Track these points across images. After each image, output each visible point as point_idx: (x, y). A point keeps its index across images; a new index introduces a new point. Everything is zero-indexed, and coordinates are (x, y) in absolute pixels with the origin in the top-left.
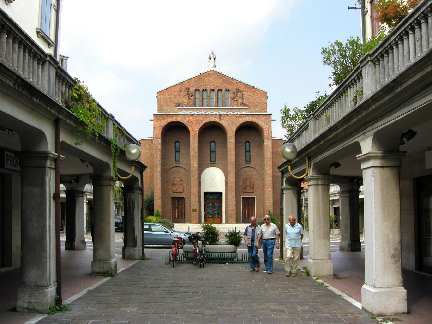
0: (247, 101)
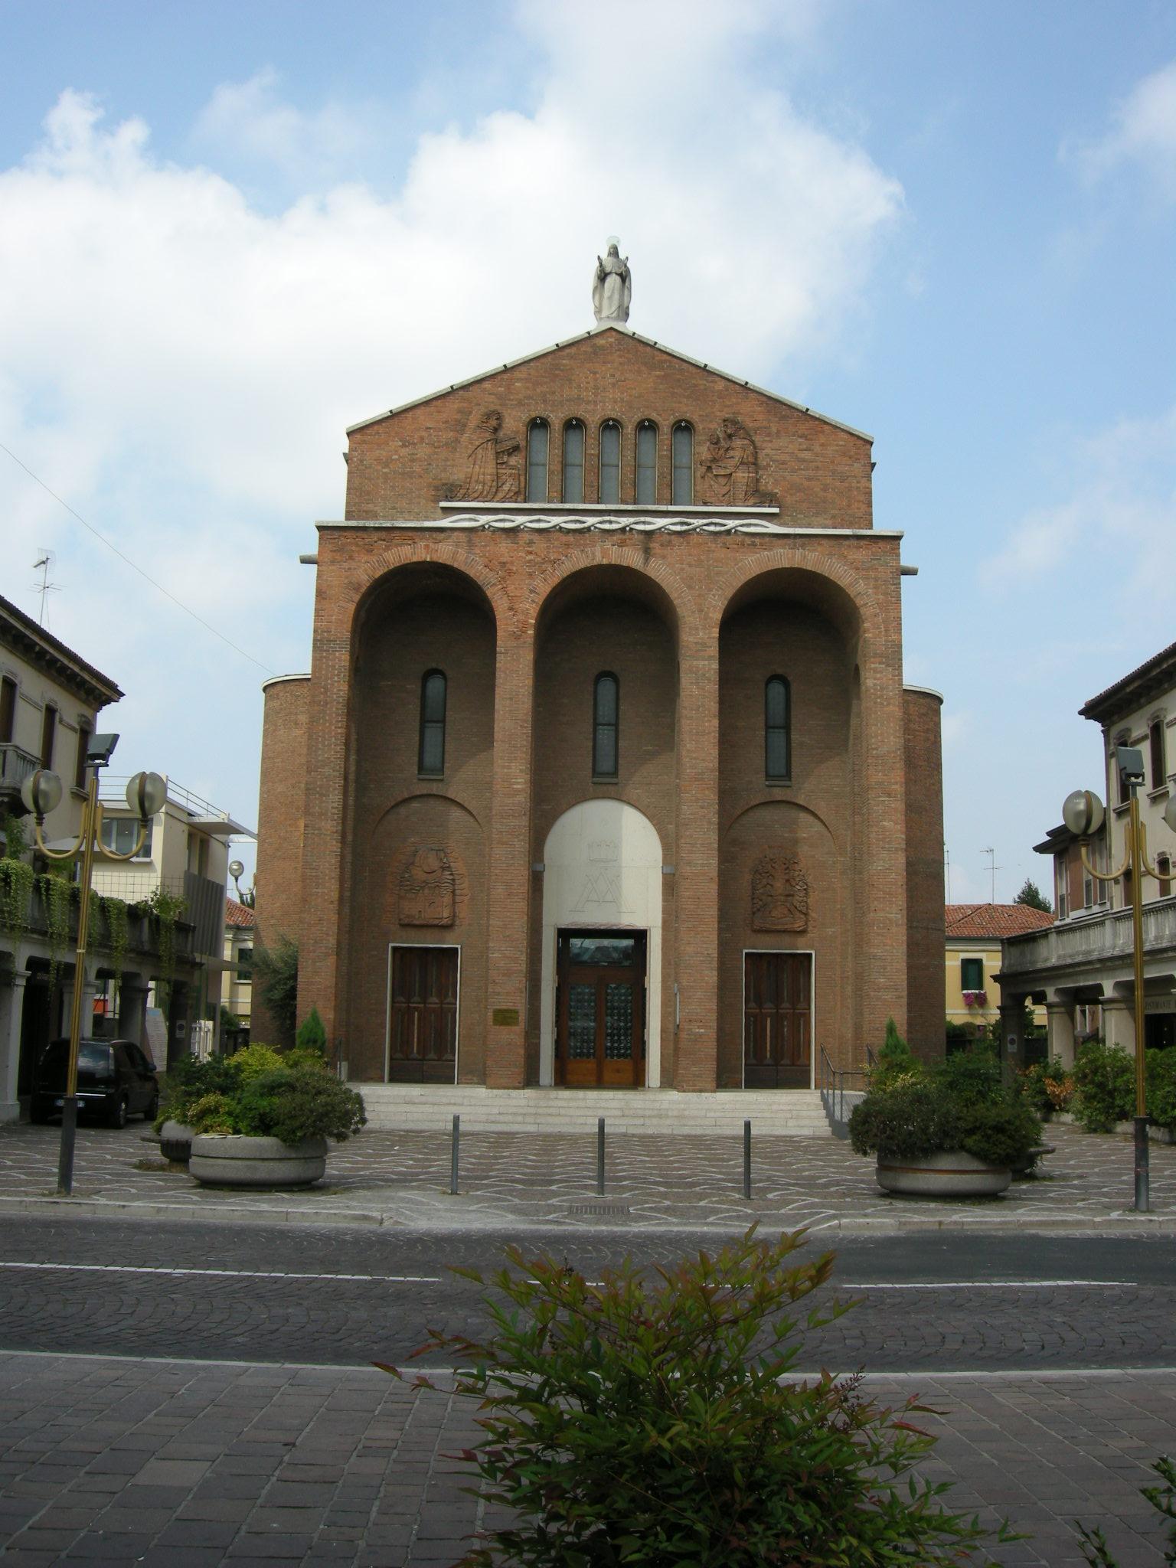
0: (776, 482)
